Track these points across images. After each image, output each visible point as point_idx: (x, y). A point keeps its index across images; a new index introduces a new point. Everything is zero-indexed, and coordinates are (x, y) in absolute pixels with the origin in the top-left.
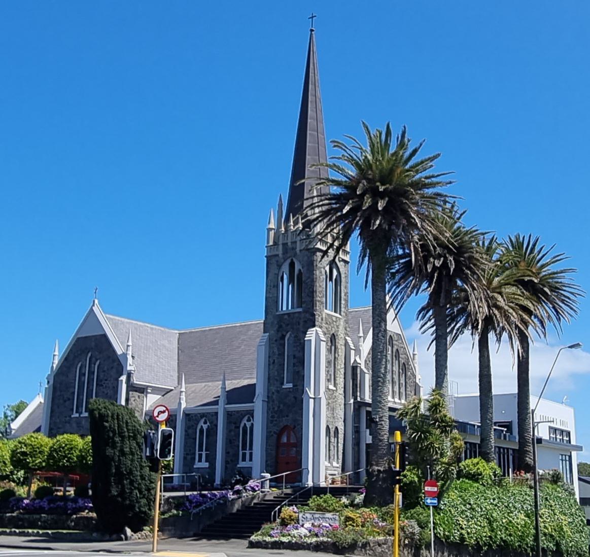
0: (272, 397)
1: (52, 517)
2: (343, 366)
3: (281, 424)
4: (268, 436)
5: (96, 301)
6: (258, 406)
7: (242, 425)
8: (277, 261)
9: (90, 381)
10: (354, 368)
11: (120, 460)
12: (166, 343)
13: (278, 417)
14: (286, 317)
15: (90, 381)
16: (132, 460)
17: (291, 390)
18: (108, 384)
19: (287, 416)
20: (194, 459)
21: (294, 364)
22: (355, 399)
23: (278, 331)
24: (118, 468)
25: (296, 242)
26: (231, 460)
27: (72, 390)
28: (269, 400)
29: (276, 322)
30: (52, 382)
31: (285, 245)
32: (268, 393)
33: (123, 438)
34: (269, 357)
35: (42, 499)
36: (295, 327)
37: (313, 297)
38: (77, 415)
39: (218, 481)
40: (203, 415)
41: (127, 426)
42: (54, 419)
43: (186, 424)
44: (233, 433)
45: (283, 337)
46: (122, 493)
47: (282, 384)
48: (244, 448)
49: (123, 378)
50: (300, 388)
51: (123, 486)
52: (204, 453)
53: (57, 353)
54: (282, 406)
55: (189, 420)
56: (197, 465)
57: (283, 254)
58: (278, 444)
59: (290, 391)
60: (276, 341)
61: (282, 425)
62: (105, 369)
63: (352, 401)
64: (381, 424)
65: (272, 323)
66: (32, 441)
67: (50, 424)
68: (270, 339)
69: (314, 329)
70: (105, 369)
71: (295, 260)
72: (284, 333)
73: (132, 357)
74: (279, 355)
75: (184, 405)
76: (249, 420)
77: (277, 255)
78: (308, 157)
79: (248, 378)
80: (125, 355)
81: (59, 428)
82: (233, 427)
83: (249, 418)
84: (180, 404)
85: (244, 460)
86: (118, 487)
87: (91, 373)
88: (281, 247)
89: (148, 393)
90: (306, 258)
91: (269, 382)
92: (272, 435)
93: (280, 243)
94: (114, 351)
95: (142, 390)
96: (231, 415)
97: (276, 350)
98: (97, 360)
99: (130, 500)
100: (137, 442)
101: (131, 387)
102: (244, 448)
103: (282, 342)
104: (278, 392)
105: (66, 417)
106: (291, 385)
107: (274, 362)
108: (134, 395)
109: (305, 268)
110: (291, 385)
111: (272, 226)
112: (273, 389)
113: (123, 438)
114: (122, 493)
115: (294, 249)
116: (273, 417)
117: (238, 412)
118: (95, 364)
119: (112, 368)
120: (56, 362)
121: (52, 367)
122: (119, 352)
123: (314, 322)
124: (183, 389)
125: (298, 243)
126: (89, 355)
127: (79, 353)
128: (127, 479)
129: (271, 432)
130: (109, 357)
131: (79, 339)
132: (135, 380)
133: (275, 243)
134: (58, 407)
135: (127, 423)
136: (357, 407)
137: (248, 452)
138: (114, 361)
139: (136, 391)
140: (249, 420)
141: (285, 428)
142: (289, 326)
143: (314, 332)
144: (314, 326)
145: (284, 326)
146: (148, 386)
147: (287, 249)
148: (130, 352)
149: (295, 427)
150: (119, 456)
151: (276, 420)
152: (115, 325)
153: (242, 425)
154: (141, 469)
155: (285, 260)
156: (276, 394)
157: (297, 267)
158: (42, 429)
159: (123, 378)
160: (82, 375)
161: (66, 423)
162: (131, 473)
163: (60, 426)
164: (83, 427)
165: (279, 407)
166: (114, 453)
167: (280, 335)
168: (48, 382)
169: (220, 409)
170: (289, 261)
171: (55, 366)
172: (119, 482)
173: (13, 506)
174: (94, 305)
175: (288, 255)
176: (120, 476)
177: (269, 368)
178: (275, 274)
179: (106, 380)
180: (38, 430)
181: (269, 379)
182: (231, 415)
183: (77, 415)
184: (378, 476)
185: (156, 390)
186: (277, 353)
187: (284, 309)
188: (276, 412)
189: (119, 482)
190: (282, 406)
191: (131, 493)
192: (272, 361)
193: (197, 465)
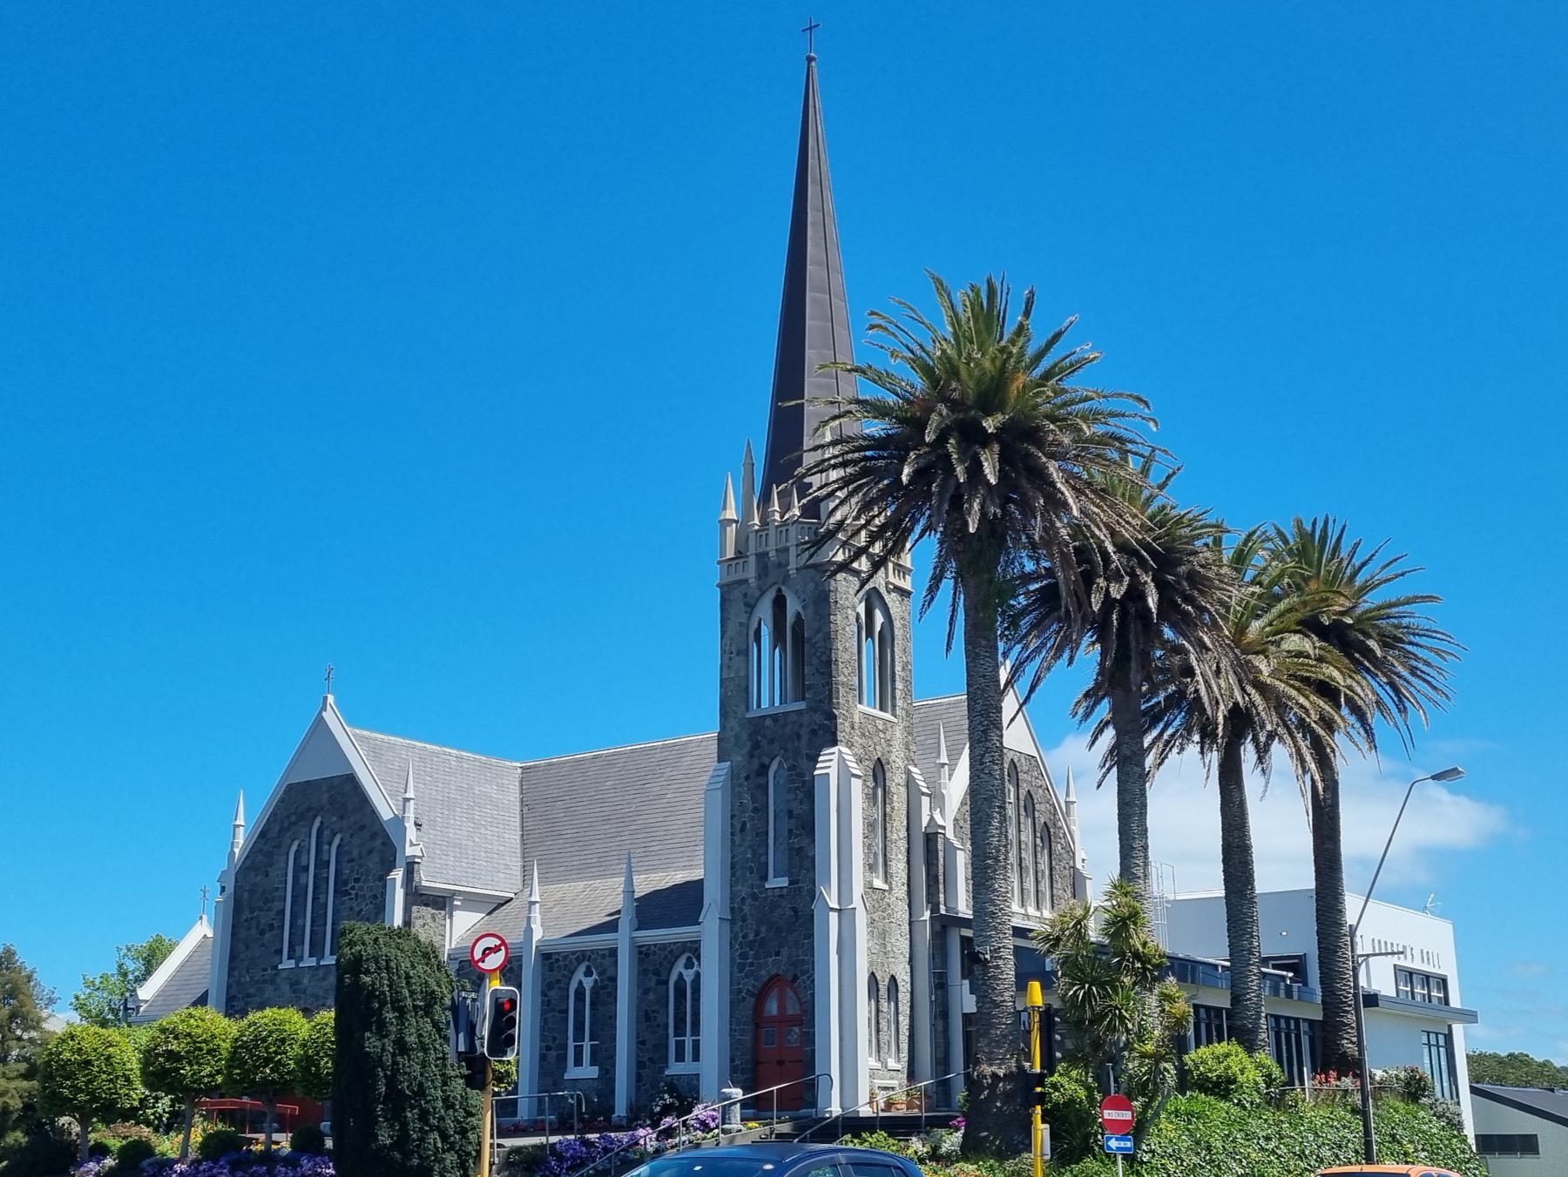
0: (741, 910)
2: (903, 834)
3: (763, 972)
4: (735, 1000)
5: (331, 699)
6: (711, 932)
7: (673, 978)
8: (745, 595)
9: (320, 882)
10: (931, 839)
11: (395, 1063)
12: (491, 789)
13: (756, 956)
14: (768, 722)
15: (320, 882)
16: (424, 1065)
17: (785, 892)
18: (361, 889)
19: (777, 954)
21: (790, 831)
24: (392, 1081)
25: (787, 549)
26: (650, 1059)
29: (745, 736)
30: (230, 889)
31: (762, 557)
32: (732, 899)
33: (401, 1012)
34: (733, 816)
35: (216, 1162)
36: (790, 746)
37: (831, 676)
39: (621, 1109)
40: (582, 956)
41: (408, 983)
42: (236, 973)
43: (544, 979)
44: (651, 996)
45: (763, 770)
46: (402, 1141)
47: (765, 878)
48: (680, 1031)
49: (398, 875)
50: (805, 886)
51: (404, 1125)
52: (587, 1045)
54: (763, 929)
56: (573, 1073)
57: (759, 577)
59: (782, 896)
60: (747, 778)
62: (355, 854)
63: (927, 915)
64: (998, 967)
65: (737, 737)
66: (189, 1026)
67: (229, 987)
68: (733, 775)
69: (835, 749)
72: (766, 761)
73: (418, 825)
74: (755, 810)
75: (538, 935)
76: (689, 965)
77: (746, 581)
80: (399, 821)
81: (249, 996)
83: (588, 968)
84: (529, 931)
85: (680, 1057)
86: (392, 1126)
87: (322, 864)
88: (752, 560)
89: (453, 908)
91: (733, 875)
92: (744, 999)
93: (752, 551)
94: (373, 813)
95: (441, 902)
96: (647, 955)
97: (747, 799)
99: (420, 1157)
100: (433, 1021)
102: (680, 1031)
103: (762, 780)
104: (754, 897)
105: (265, 970)
106: (783, 882)
107: (743, 829)
109: (810, 610)
111: (731, 513)
112: (744, 891)
113: (401, 1012)
114: (402, 1141)
115: (782, 565)
116: (743, 956)
117: (663, 947)
118: (330, 844)
119: (371, 852)
121: (232, 853)
123: (835, 734)
125: (793, 552)
127: (293, 818)
128: (413, 1107)
129: (740, 991)
130: (363, 827)
131: (290, 787)
132: (427, 879)
133: (740, 554)
134: (247, 948)
135: (408, 977)
136: (938, 927)
137: (688, 1041)
138: (374, 836)
139: (426, 905)
140: (689, 965)
141: (774, 980)
142: (776, 744)
143: (835, 757)
144: (834, 743)
145: (764, 743)
146: (454, 893)
148: (411, 815)
149: (795, 978)
150: (394, 1055)
151: (752, 964)
152: (376, 752)
153: (673, 978)
154: (445, 1084)
155: (763, 593)
156: (749, 901)
157: (792, 607)
159: (398, 875)
160: (301, 869)
161: (265, 982)
162: (421, 1092)
163: (252, 991)
164: (304, 992)
165: (757, 933)
166: (383, 1049)
167: (756, 763)
168: (223, 889)
169: (623, 942)
171: (237, 851)
172: (396, 1115)
175: (770, 580)
176: (397, 1101)
178: (741, 624)
179: (357, 880)
180: (202, 1001)
182: (647, 955)
184: (993, 1087)
185: (473, 901)
186: (751, 807)
187: (765, 704)
188: (751, 945)
189: (396, 1115)
191: (422, 1140)
192: (738, 827)
193: (573, 1073)
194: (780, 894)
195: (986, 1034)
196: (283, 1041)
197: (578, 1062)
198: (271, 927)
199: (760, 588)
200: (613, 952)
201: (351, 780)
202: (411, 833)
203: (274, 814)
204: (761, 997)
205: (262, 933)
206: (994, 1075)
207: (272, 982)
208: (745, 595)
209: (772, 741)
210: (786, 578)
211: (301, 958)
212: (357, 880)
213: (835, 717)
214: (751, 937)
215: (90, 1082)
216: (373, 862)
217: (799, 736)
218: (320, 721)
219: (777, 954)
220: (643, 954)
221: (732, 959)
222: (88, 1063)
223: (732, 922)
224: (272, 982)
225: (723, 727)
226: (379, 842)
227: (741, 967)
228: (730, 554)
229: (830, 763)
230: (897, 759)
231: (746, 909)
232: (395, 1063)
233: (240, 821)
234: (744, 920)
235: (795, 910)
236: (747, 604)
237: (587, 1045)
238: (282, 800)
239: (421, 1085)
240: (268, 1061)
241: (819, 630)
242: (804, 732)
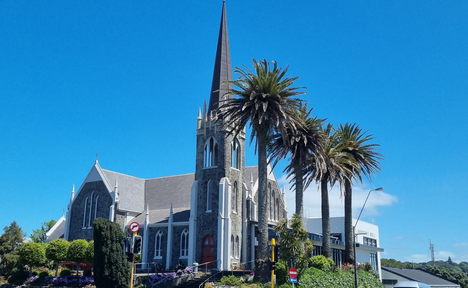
4: (197, 240)
5: (97, 161)
6: (192, 223)
10: (248, 201)
11: (110, 254)
13: (203, 230)
14: (208, 171)
16: (117, 255)
19: (208, 229)
20: (154, 254)
22: (249, 219)
23: (203, 179)
24: (109, 259)
25: (214, 127)
27: (82, 213)
28: (198, 219)
29: (202, 174)
30: (70, 209)
31: (208, 129)
35: (64, 278)
36: (213, 177)
37: (224, 159)
38: (85, 228)
39: (168, 267)
40: (159, 228)
41: (116, 234)
44: (176, 239)
45: (206, 183)
47: (206, 210)
49: (113, 206)
52: (159, 251)
53: (73, 192)
54: (205, 223)
55: (151, 231)
56: (156, 258)
57: (207, 134)
58: (203, 246)
60: (202, 184)
61: (205, 234)
62: (102, 200)
63: (246, 221)
68: (199, 184)
69: (224, 178)
70: (102, 200)
71: (213, 138)
74: (204, 193)
75: (148, 223)
78: (221, 77)
79: (186, 207)
80: (113, 193)
82: (177, 235)
84: (146, 222)
87: (94, 203)
88: (205, 130)
89: (127, 215)
91: (198, 209)
93: (205, 127)
95: (123, 214)
97: (82, 194)
98: (97, 196)
99: (116, 278)
100: (121, 244)
101: (118, 212)
104: (203, 215)
106: (210, 211)
107: (201, 197)
108: (119, 216)
109: (219, 143)
110: (210, 211)
112: (200, 213)
113: (112, 241)
119: (106, 200)
120: (73, 196)
121: (71, 200)
122: (110, 191)
124: (148, 213)
126: (93, 193)
130: (104, 194)
132: (120, 208)
133: (202, 128)
138: (107, 196)
141: (207, 236)
144: (224, 176)
145: (207, 176)
146: (127, 211)
147: (208, 131)
148: (117, 191)
150: (110, 252)
152: (108, 175)
153: (182, 234)
154: (123, 260)
155: (208, 138)
156: (202, 216)
157: (215, 142)
158: (65, 236)
159: (113, 206)
162: (116, 262)
165: (203, 224)
166: (107, 251)
167: (204, 181)
168: (68, 209)
170: (209, 139)
173: (47, 282)
174: (95, 164)
175: (210, 135)
176: (110, 264)
177: (198, 200)
179: (102, 207)
180: (62, 237)
181: (198, 207)
183: (85, 228)
185: (132, 214)
187: (207, 166)
190: (205, 223)
191: (116, 274)
192: (199, 197)
193: (156, 258)
194: (210, 214)
195: (261, 251)
196: (82, 248)
197: (157, 255)
198: (80, 218)
199: (207, 136)
200: (167, 227)
201: (102, 182)
202: (117, 196)
203: (82, 190)
204: (204, 240)
205: (78, 220)
206: (262, 262)
207: (80, 232)
209: (208, 176)
210: (213, 135)
211: (88, 227)
212: (102, 207)
213: (225, 170)
215: (33, 256)
216: (107, 203)
217: (215, 174)
218: (94, 167)
220: (174, 228)
221: (197, 230)
222: (32, 252)
223: (197, 221)
224: (80, 232)
225: (196, 171)
226: (108, 198)
227: (199, 232)
228: (200, 128)
229: (223, 181)
230: (240, 181)
231: (201, 218)
232: (110, 254)
233: (73, 192)
234: (200, 220)
235: (213, 218)
236: (203, 141)
237: (159, 251)
238: (84, 186)
239: (116, 260)
240: (78, 252)
241: (221, 148)
242: (217, 173)
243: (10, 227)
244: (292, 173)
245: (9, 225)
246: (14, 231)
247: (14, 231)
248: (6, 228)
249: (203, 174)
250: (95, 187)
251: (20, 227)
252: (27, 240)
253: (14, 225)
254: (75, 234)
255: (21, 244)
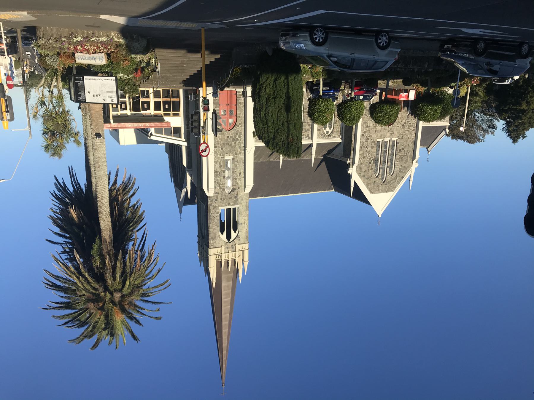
1: (251, 66)
13: (235, 137)
23: (237, 194)
29: (239, 200)
36: (224, 197)
54: (233, 144)
60: (239, 188)
62: (370, 171)
70: (370, 171)
71: (227, 241)
90: (217, 242)
103: (234, 187)
104: (236, 154)
110: (226, 158)
130: (368, 179)
138: (364, 176)
147: (232, 248)
156: (238, 153)
165: (235, 143)
167: (236, 192)
179: (370, 163)
190: (233, 144)
198: (400, 150)
205: (403, 149)
208: (239, 240)
212: (370, 163)
214: (237, 142)
216: (364, 168)
217: (221, 199)
219: (228, 137)
226: (363, 174)
243: (519, 138)
244: (59, 208)
245: (520, 140)
246: (515, 133)
247: (515, 133)
248: (524, 137)
249: (237, 200)
250: (380, 188)
251: (509, 137)
252: (500, 124)
253: (515, 140)
254: (407, 132)
255: (508, 120)
